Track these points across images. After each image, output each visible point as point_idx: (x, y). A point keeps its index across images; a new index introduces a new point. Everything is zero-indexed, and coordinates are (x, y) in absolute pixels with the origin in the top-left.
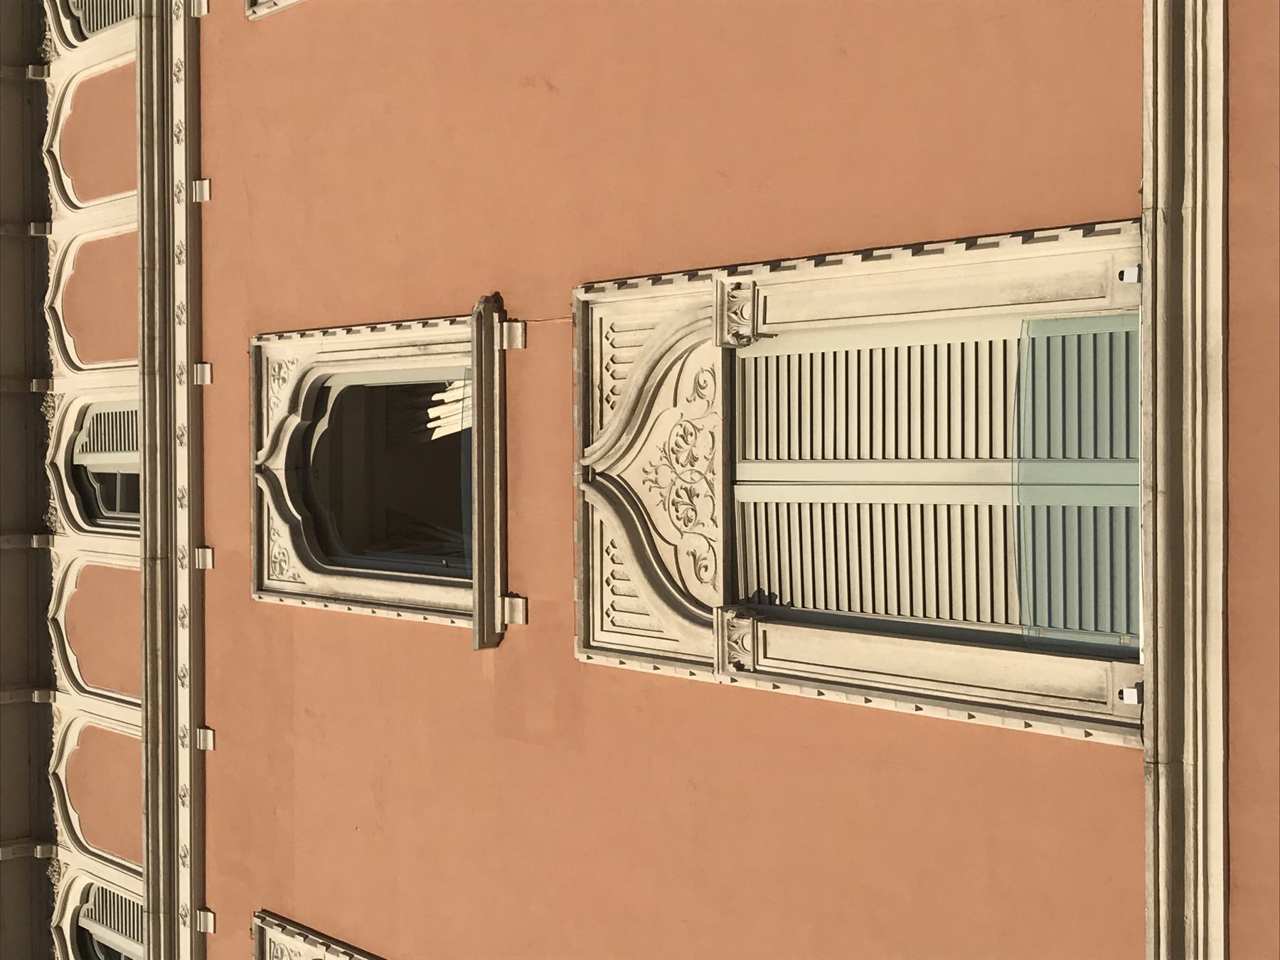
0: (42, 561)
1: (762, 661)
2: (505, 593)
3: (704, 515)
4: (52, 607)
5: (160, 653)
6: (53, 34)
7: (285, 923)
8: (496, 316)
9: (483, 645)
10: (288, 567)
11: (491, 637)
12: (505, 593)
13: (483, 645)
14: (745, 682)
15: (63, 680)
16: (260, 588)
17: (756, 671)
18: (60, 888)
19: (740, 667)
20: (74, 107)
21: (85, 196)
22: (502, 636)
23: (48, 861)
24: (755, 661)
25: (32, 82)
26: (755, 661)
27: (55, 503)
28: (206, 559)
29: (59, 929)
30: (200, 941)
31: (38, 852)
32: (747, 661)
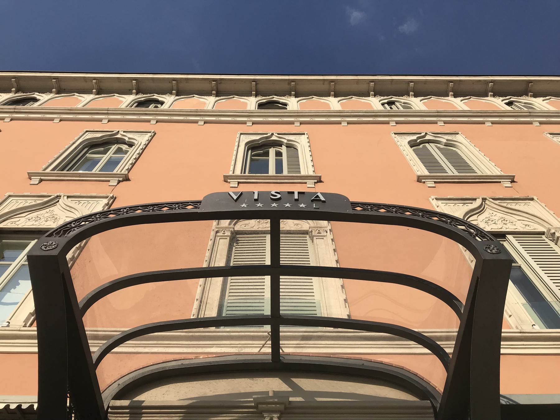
0: (249, 94)
1: (219, 238)
2: (239, 183)
3: (261, 226)
4: (38, 94)
5: (548, 119)
6: (382, 98)
7: (152, 137)
8: (121, 179)
9: (28, 173)
10: (246, 139)
11: (30, 176)
12: (239, 183)
13: (28, 173)
14: (213, 234)
15: (218, 98)
16: (241, 134)
17: (216, 236)
18: (164, 96)
19: (217, 232)
20: (364, 102)
21: (300, 104)
22: (227, 182)
23: (171, 93)
24: (218, 236)
25: (369, 94)
26: (218, 236)
27: (263, 98)
28: (57, 121)
29: (392, 98)
30: (3, 119)
31: (134, 91)
32: (218, 234)
